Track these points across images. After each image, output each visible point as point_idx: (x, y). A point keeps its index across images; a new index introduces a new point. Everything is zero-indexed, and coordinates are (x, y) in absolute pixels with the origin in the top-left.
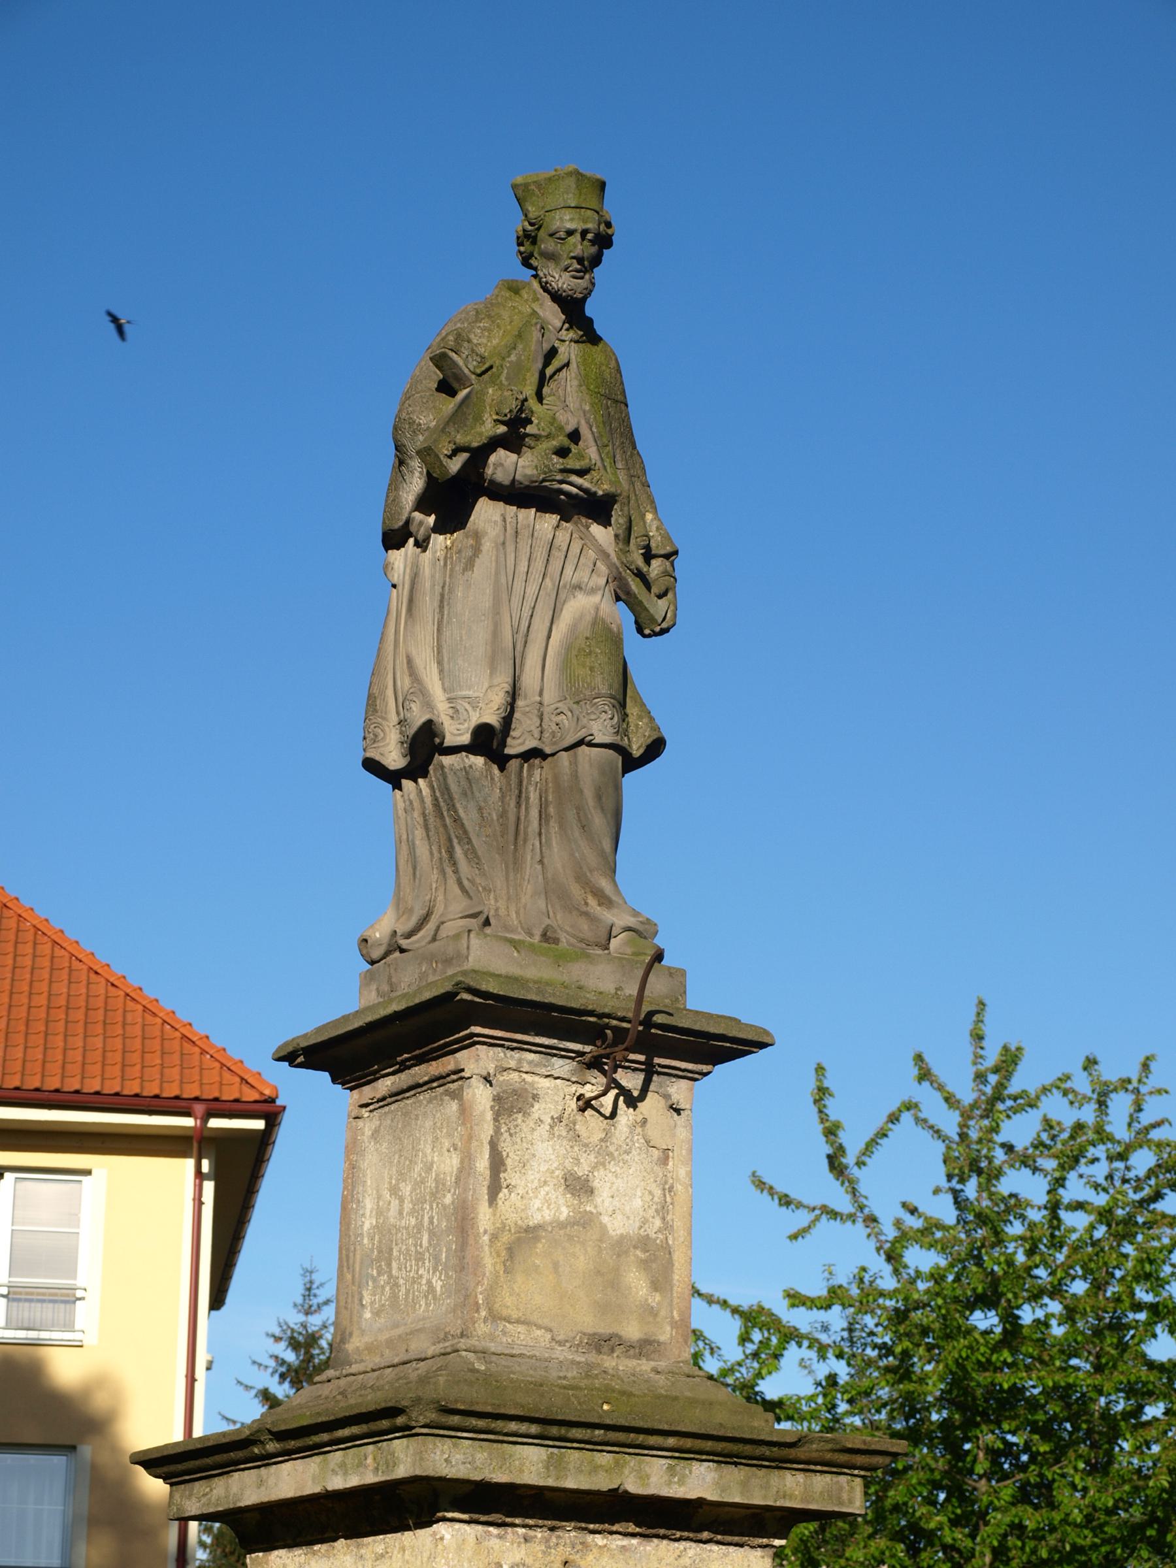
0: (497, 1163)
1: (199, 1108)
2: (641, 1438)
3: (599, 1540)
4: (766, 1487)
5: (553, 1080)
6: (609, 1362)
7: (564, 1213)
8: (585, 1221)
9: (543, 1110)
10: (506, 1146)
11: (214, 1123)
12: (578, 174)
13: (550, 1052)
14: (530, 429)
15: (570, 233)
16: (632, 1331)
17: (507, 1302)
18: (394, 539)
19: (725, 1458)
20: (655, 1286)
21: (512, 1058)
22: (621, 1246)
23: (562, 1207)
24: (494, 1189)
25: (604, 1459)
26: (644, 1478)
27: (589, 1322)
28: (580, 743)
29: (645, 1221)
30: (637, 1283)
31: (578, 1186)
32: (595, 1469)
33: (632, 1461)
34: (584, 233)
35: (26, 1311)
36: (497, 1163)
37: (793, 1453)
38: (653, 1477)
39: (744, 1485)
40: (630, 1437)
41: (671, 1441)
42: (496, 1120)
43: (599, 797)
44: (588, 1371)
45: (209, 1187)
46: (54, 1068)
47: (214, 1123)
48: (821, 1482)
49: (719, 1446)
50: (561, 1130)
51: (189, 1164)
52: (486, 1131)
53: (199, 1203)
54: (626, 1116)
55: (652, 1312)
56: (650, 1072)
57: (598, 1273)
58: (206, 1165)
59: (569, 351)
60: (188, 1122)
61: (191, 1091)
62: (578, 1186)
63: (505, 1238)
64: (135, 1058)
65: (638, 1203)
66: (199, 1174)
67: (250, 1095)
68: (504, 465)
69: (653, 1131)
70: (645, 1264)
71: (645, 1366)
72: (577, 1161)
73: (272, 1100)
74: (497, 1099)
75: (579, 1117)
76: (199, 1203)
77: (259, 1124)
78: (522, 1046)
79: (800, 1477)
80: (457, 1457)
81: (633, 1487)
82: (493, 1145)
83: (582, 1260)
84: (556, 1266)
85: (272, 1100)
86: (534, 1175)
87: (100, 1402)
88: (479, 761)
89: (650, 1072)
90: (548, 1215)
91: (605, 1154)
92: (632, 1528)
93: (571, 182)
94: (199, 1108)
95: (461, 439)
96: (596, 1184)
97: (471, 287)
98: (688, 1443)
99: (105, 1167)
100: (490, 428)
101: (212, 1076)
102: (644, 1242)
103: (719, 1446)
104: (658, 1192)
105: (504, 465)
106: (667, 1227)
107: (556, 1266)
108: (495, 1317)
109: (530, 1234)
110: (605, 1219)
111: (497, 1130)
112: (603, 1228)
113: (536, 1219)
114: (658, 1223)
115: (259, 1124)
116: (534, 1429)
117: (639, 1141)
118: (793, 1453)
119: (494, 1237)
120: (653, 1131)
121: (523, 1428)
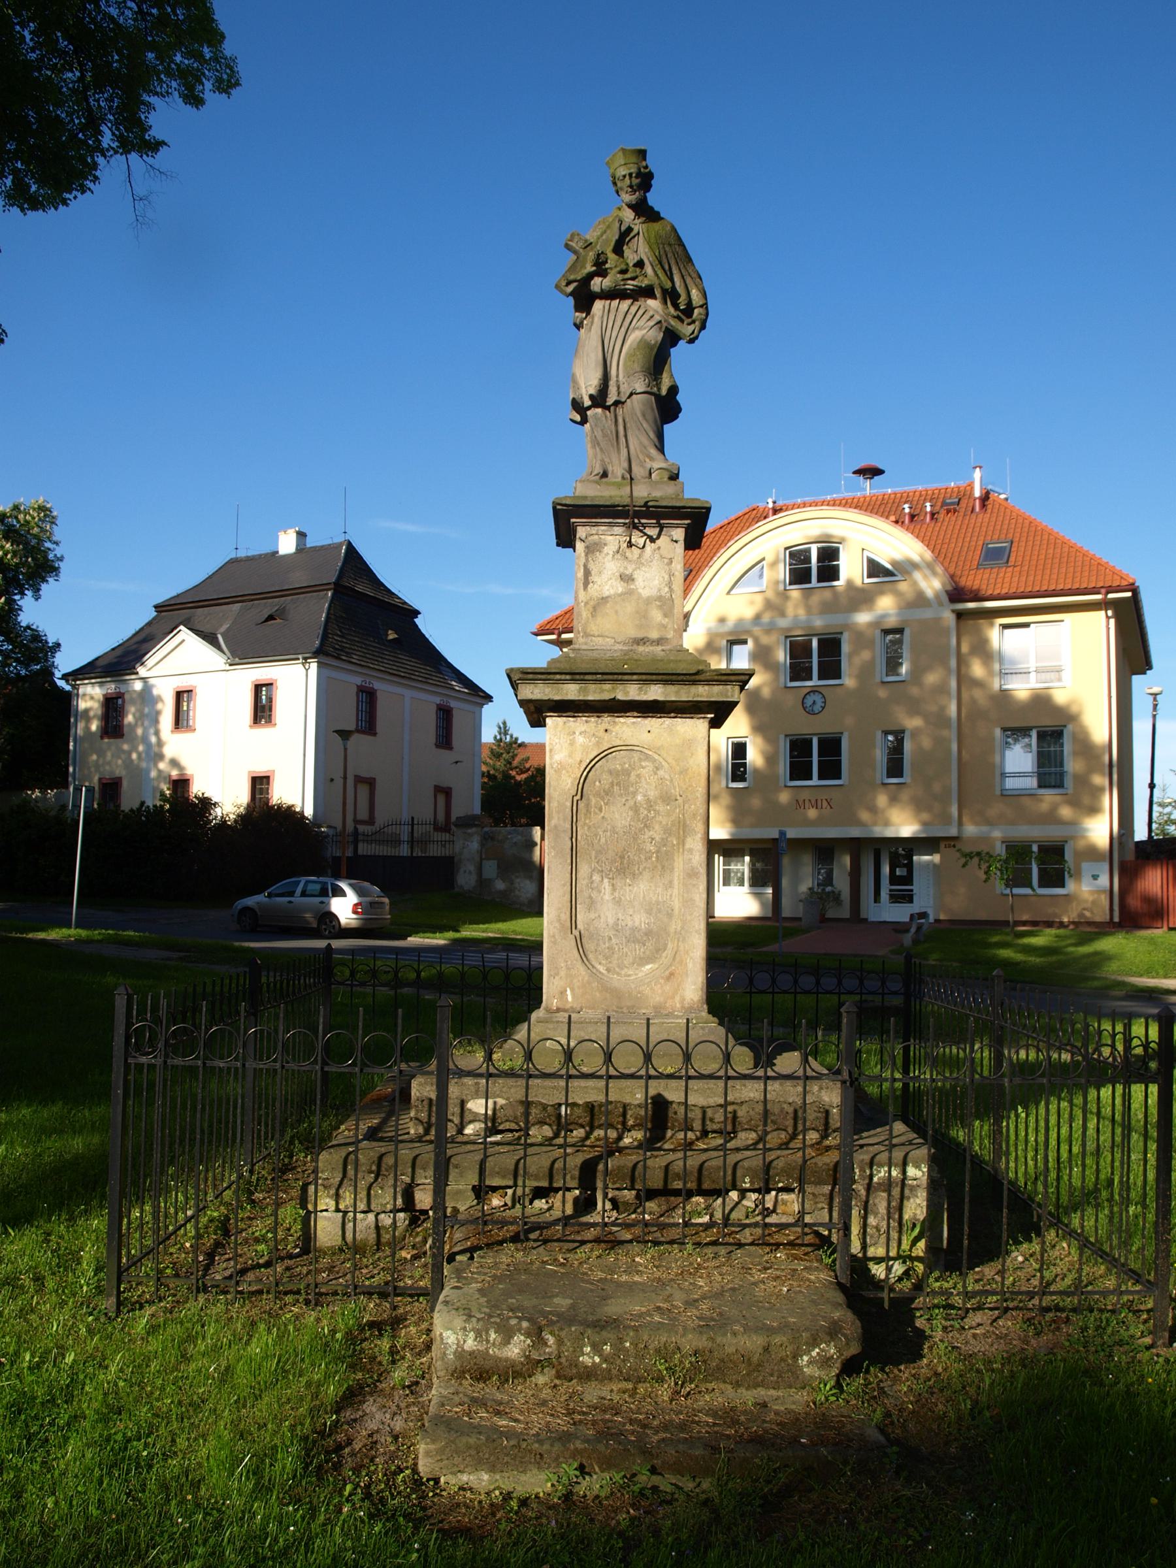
0: (587, 573)
1: (1103, 591)
2: (620, 677)
3: (622, 720)
4: (689, 693)
5: (612, 537)
6: (641, 649)
7: (620, 590)
8: (630, 593)
9: (610, 549)
10: (591, 566)
11: (1110, 596)
12: (623, 150)
13: (610, 525)
14: (607, 266)
15: (624, 176)
16: (654, 635)
17: (593, 628)
18: (578, 326)
19: (666, 682)
20: (665, 615)
21: (594, 530)
22: (648, 601)
23: (620, 587)
24: (586, 584)
25: (607, 686)
26: (627, 693)
27: (633, 633)
28: (631, 394)
29: (659, 590)
30: (657, 616)
31: (627, 578)
32: (602, 691)
33: (621, 687)
34: (630, 175)
35: (1044, 676)
36: (587, 573)
37: (697, 678)
38: (632, 692)
39: (677, 693)
40: (616, 676)
41: (635, 677)
42: (586, 555)
43: (644, 416)
44: (626, 653)
45: (1112, 621)
46: (1045, 582)
47: (1110, 596)
48: (717, 689)
49: (665, 677)
50: (618, 556)
51: (1103, 612)
52: (583, 560)
53: (1108, 629)
54: (650, 547)
55: (665, 627)
56: (661, 527)
57: (637, 612)
58: (1110, 613)
59: (638, 226)
60: (1099, 597)
61: (1100, 584)
62: (627, 578)
63: (592, 603)
64: (1078, 574)
65: (656, 582)
66: (1108, 617)
67: (1124, 583)
68: (597, 284)
69: (663, 552)
70: (660, 607)
71: (660, 648)
72: (626, 568)
73: (1133, 584)
74: (587, 547)
75: (628, 550)
76: (1108, 629)
77: (1129, 594)
78: (597, 524)
79: (706, 688)
80: (536, 691)
81: (621, 696)
82: (585, 566)
83: (630, 607)
84: (616, 612)
85: (1133, 584)
86: (605, 577)
87: (1074, 709)
88: (599, 410)
89: (661, 527)
90: (612, 592)
91: (639, 563)
92: (636, 714)
93: (621, 154)
94: (1103, 591)
95: (572, 277)
96: (635, 576)
97: (604, 213)
98: (644, 677)
99: (1067, 617)
100: (589, 268)
101: (1109, 578)
102: (660, 598)
103: (665, 677)
104: (667, 577)
105: (597, 284)
106: (671, 590)
107: (616, 612)
108: (587, 635)
109: (604, 600)
110: (640, 591)
111: (587, 560)
112: (640, 594)
113: (606, 594)
114: (667, 589)
115: (1129, 594)
116: (568, 677)
117: (657, 556)
118: (697, 678)
119: (586, 604)
120: (663, 552)
121: (563, 677)
